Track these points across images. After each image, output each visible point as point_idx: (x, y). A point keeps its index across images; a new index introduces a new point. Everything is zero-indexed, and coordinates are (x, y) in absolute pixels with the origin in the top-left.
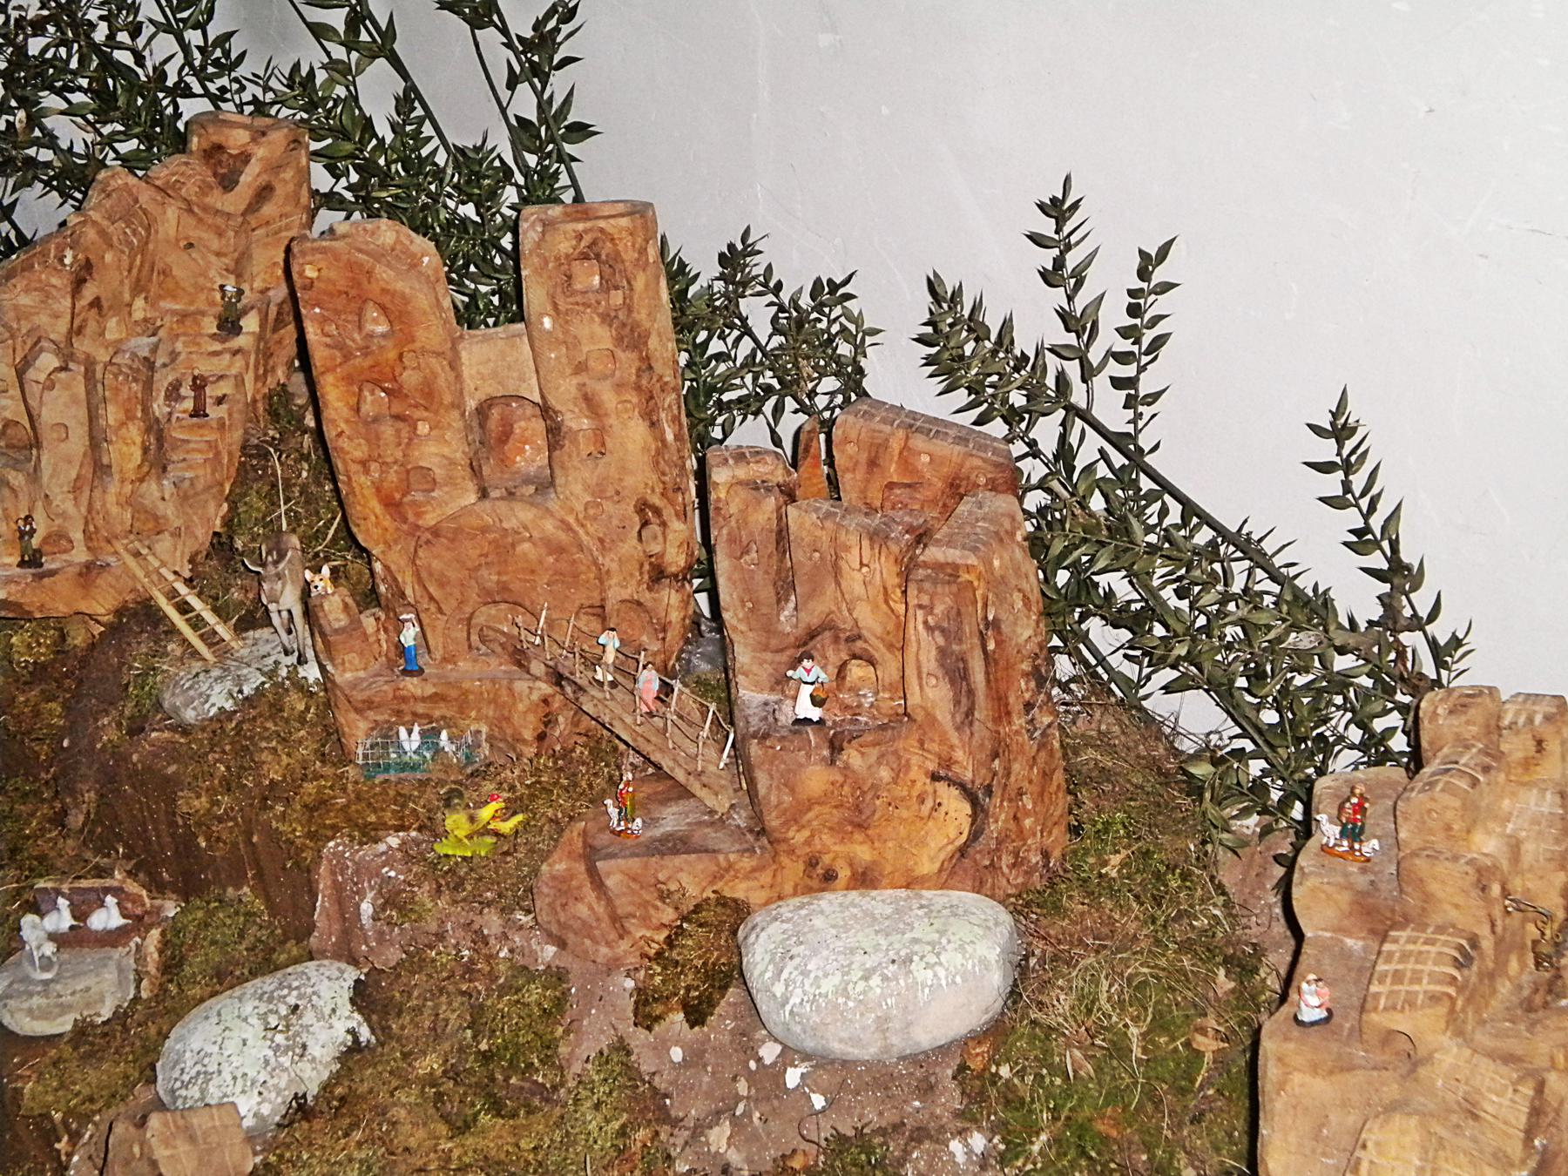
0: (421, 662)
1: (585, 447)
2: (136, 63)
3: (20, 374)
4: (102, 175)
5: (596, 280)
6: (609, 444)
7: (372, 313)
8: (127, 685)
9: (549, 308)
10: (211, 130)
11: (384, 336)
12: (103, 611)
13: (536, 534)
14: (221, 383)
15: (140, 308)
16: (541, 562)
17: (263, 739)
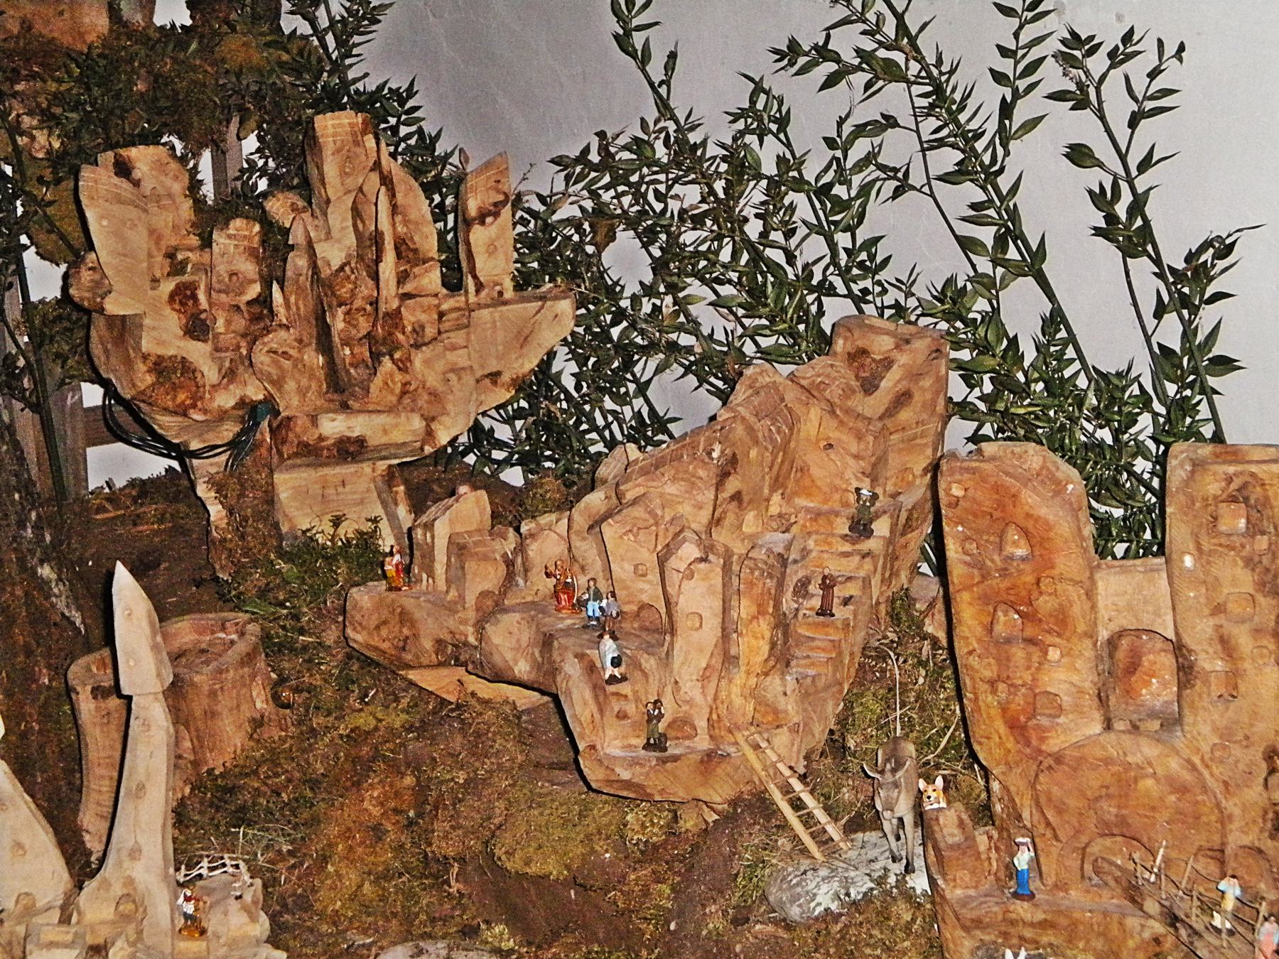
0: (1032, 888)
1: (1216, 688)
2: (788, 263)
3: (662, 562)
4: (749, 372)
5: (1242, 523)
6: (1242, 688)
7: (1013, 535)
8: (736, 875)
9: (1192, 546)
10: (856, 335)
11: (1023, 559)
12: (718, 799)
13: (1160, 772)
14: (849, 584)
15: (776, 504)
16: (1161, 799)
17: (868, 945)
